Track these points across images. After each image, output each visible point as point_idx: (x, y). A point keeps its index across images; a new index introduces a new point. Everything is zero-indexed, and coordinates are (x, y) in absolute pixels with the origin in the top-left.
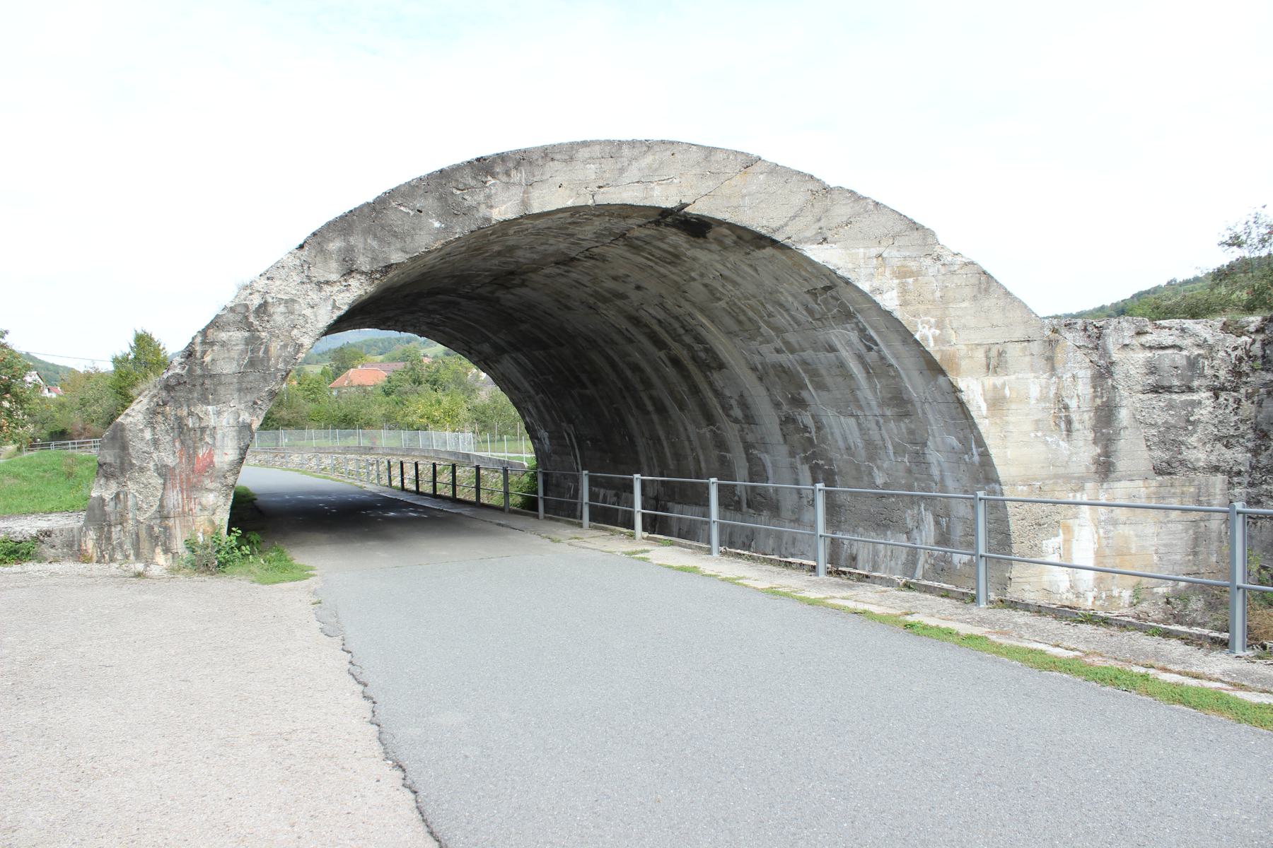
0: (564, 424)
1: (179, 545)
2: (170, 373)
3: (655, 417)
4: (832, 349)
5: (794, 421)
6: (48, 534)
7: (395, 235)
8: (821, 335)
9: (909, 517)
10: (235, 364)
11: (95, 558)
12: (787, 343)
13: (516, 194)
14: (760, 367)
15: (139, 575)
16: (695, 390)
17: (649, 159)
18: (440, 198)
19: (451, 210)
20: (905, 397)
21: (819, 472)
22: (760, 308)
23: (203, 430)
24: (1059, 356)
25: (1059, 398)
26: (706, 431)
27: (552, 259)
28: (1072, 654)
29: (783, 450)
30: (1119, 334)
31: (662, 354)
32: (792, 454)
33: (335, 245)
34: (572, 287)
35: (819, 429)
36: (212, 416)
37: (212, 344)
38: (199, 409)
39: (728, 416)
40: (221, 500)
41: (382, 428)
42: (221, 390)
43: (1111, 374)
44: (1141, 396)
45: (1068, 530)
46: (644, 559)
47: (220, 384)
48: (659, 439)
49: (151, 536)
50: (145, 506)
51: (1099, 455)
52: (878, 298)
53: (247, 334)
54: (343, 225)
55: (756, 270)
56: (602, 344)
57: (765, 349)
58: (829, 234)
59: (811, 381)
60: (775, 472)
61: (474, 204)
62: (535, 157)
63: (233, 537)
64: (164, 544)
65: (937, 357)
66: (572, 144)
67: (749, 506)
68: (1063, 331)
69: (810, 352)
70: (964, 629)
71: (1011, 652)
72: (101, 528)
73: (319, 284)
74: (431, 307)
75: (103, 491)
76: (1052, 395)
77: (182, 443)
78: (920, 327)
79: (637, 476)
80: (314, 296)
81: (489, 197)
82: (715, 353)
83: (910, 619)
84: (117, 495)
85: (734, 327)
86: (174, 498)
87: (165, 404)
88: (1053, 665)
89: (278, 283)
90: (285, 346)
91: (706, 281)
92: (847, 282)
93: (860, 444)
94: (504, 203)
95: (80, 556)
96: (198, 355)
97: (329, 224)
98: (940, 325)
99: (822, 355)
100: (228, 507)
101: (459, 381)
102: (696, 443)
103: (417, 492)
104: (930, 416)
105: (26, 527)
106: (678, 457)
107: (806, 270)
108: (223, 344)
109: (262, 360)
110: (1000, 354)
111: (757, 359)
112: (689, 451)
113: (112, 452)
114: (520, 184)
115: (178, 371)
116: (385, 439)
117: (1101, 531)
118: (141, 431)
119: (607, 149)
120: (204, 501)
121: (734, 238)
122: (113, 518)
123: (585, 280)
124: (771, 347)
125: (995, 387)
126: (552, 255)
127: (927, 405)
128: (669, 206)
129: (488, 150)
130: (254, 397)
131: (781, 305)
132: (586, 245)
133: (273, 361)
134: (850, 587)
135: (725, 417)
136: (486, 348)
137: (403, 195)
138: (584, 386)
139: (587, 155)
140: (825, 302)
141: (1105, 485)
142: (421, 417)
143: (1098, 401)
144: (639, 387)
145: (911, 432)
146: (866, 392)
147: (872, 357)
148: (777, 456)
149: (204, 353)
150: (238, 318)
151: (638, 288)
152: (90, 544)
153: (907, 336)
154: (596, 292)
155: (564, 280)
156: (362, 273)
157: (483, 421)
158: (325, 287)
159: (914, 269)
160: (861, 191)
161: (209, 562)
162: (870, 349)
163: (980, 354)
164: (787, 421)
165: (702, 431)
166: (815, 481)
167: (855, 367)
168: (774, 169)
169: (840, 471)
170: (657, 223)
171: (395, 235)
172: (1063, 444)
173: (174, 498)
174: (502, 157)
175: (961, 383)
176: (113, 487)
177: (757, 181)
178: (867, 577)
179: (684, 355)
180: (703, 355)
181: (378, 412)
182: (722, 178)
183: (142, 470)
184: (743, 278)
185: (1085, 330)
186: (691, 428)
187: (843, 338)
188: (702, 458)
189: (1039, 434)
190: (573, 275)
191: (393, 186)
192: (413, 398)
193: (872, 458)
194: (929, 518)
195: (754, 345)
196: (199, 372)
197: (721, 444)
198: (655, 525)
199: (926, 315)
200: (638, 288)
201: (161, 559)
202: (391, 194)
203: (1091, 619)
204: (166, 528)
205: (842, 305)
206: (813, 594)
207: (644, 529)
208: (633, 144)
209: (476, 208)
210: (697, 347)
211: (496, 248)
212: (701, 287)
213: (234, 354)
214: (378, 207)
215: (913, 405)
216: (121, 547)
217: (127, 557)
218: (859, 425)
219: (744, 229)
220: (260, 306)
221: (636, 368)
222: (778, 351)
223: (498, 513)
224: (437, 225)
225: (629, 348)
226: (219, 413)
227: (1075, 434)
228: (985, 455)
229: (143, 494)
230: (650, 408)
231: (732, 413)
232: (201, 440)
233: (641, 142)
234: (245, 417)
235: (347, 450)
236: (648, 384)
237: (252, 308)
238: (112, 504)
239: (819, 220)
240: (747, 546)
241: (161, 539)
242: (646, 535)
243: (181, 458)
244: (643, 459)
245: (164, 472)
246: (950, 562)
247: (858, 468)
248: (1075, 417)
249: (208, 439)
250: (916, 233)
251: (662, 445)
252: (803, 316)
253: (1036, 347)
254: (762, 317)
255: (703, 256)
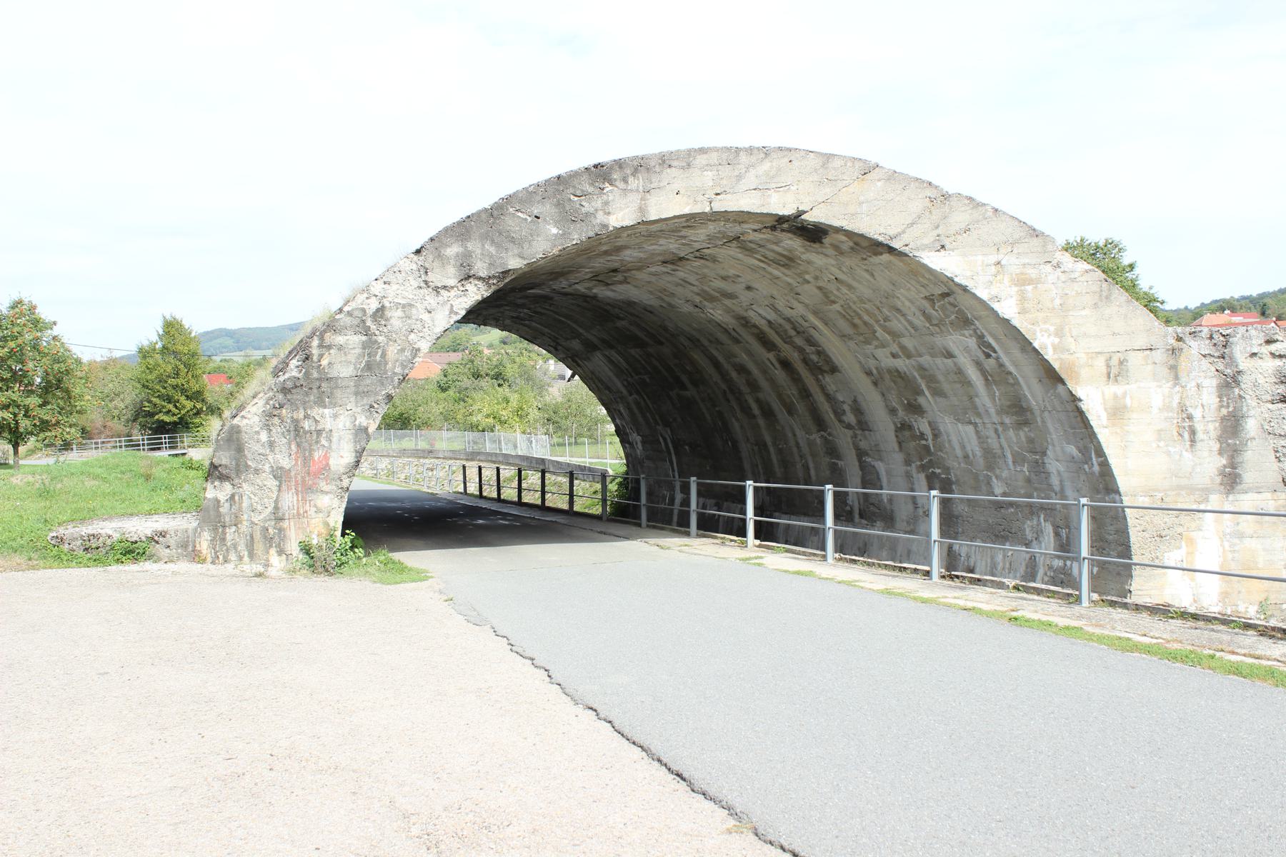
0: (659, 428)
1: (293, 547)
2: (287, 376)
3: (761, 422)
4: (950, 355)
5: (910, 427)
6: (163, 534)
7: (513, 240)
8: (938, 341)
9: (1028, 527)
10: (352, 367)
11: (209, 559)
12: (903, 348)
13: (634, 199)
14: (875, 372)
15: (260, 575)
16: (805, 394)
17: (766, 166)
18: (558, 204)
19: (569, 217)
20: (1024, 405)
21: (936, 481)
22: (877, 312)
23: (319, 432)
24: (1183, 364)
25: (1183, 408)
26: (816, 437)
27: (661, 258)
28: (1154, 641)
29: (899, 457)
30: (1248, 340)
31: (771, 356)
32: (908, 462)
33: (453, 250)
34: (677, 285)
35: (936, 436)
36: (328, 419)
37: (329, 347)
38: (316, 412)
39: (841, 421)
40: (336, 502)
41: (440, 429)
42: (338, 393)
43: (1237, 383)
44: (1270, 406)
45: (1191, 542)
46: (759, 565)
47: (337, 387)
48: (765, 445)
49: (265, 537)
50: (259, 508)
51: (1225, 466)
52: (996, 306)
53: (364, 338)
54: (461, 230)
55: (872, 275)
56: (706, 343)
57: (880, 353)
58: (946, 242)
59: (929, 388)
60: (889, 482)
61: (592, 210)
62: (653, 164)
63: (347, 539)
64: (278, 546)
65: (1056, 365)
66: (689, 151)
67: (861, 516)
68: (1188, 339)
69: (927, 357)
70: (1062, 622)
71: (1100, 639)
72: (215, 529)
73: (436, 289)
74: (520, 301)
75: (218, 492)
76: (1175, 404)
77: (298, 445)
78: (1039, 335)
79: (749, 483)
80: (431, 300)
81: (606, 203)
82: (828, 356)
83: (1015, 614)
84: (233, 496)
85: (849, 330)
86: (289, 500)
87: (281, 407)
88: (1136, 648)
89: (394, 287)
90: (403, 350)
91: (820, 284)
92: (965, 289)
93: (979, 453)
94: (621, 209)
95: (196, 557)
96: (315, 358)
97: (446, 230)
98: (1059, 333)
99: (941, 362)
100: (342, 510)
101: (528, 377)
102: (805, 450)
103: (499, 500)
104: (1050, 425)
105: (139, 527)
106: (785, 464)
107: (923, 277)
108: (340, 348)
109: (379, 364)
110: (1121, 363)
111: (872, 364)
112: (797, 459)
113: (227, 454)
114: (637, 191)
115: (295, 373)
116: (447, 440)
117: (1226, 544)
118: (258, 433)
119: (725, 156)
120: (319, 503)
121: (851, 244)
122: (227, 519)
123: (692, 279)
124: (886, 351)
125: (1116, 397)
126: (660, 254)
127: (1046, 414)
128: (786, 213)
129: (605, 157)
130: (371, 400)
131: (898, 310)
132: (697, 246)
133: (390, 365)
134: (961, 588)
135: (837, 423)
136: (576, 345)
137: (521, 201)
138: (686, 389)
139: (704, 162)
140: (943, 308)
141: (1231, 497)
142: (488, 416)
143: (1224, 411)
144: (745, 389)
145: (1031, 441)
146: (984, 398)
147: (990, 364)
148: (891, 464)
149: (321, 356)
150: (356, 322)
151: (749, 288)
152: (204, 545)
153: (1026, 345)
154: (703, 290)
155: (670, 278)
156: (480, 278)
157: (554, 420)
158: (442, 292)
159: (1033, 276)
160: (979, 198)
161: (315, 561)
162: (988, 356)
163: (1100, 363)
164: (903, 427)
165: (812, 437)
166: (931, 488)
167: (973, 374)
168: (893, 176)
169: (958, 481)
170: (773, 228)
171: (513, 240)
172: (1187, 455)
173: (289, 500)
174: (620, 164)
175: (1079, 392)
176: (227, 486)
177: (874, 188)
178: (979, 580)
179: (794, 357)
180: (814, 358)
181: (436, 409)
182: (840, 184)
183: (257, 471)
184: (860, 282)
185: (1211, 338)
186: (800, 434)
187: (961, 343)
188: (811, 465)
189: (1162, 444)
190: (681, 274)
191: (511, 192)
192: (477, 395)
193: (990, 467)
194: (1049, 529)
195: (869, 349)
196: (315, 375)
197: (833, 451)
198: (764, 533)
199: (1045, 322)
200: (749, 288)
201: (275, 559)
202: (509, 200)
203: (1184, 615)
204: (281, 530)
205: (960, 312)
206: (926, 594)
207: (756, 537)
208: (750, 150)
209: (594, 215)
210: (809, 349)
211: (605, 248)
212: (817, 291)
213: (352, 358)
214: (495, 213)
215: (1033, 413)
216: (235, 548)
217: (241, 558)
218: (977, 432)
219: (862, 236)
220: (378, 310)
221: (742, 369)
222: (894, 356)
223: (595, 521)
224: (554, 231)
225: (736, 349)
226: (335, 416)
227: (1199, 445)
228: (1105, 465)
229: (255, 496)
230: (756, 411)
231: (845, 418)
232: (317, 442)
233: (758, 149)
234: (362, 420)
235: (403, 453)
236: (754, 386)
237: (370, 312)
238: (227, 505)
239: (937, 227)
240: (862, 552)
241: (275, 540)
242: (758, 542)
243: (296, 460)
244: (747, 466)
245: (280, 475)
246: (1070, 575)
247: (976, 477)
248: (1199, 427)
249: (324, 442)
250: (1035, 239)
251: (768, 452)
252: (919, 321)
253: (1159, 356)
254: (877, 321)
255: (818, 260)
